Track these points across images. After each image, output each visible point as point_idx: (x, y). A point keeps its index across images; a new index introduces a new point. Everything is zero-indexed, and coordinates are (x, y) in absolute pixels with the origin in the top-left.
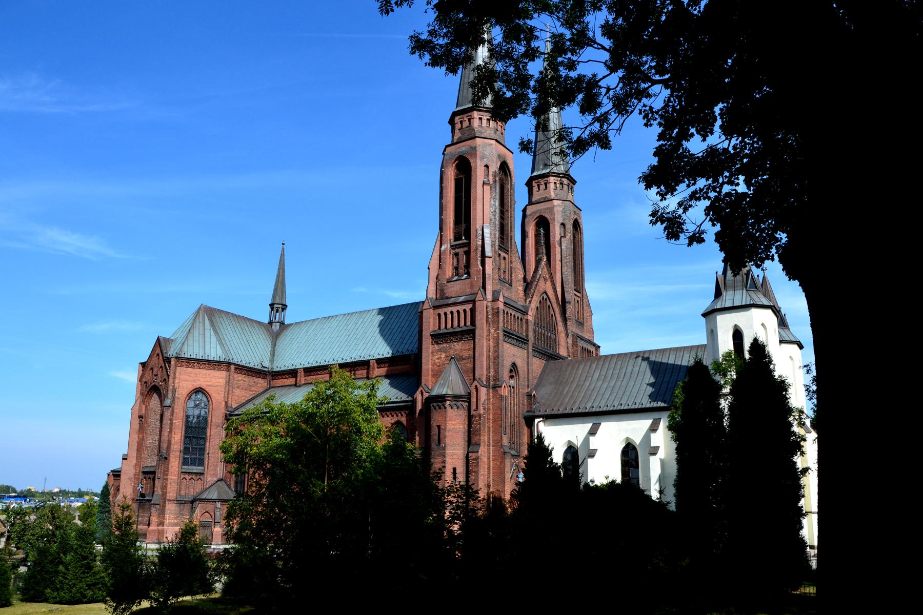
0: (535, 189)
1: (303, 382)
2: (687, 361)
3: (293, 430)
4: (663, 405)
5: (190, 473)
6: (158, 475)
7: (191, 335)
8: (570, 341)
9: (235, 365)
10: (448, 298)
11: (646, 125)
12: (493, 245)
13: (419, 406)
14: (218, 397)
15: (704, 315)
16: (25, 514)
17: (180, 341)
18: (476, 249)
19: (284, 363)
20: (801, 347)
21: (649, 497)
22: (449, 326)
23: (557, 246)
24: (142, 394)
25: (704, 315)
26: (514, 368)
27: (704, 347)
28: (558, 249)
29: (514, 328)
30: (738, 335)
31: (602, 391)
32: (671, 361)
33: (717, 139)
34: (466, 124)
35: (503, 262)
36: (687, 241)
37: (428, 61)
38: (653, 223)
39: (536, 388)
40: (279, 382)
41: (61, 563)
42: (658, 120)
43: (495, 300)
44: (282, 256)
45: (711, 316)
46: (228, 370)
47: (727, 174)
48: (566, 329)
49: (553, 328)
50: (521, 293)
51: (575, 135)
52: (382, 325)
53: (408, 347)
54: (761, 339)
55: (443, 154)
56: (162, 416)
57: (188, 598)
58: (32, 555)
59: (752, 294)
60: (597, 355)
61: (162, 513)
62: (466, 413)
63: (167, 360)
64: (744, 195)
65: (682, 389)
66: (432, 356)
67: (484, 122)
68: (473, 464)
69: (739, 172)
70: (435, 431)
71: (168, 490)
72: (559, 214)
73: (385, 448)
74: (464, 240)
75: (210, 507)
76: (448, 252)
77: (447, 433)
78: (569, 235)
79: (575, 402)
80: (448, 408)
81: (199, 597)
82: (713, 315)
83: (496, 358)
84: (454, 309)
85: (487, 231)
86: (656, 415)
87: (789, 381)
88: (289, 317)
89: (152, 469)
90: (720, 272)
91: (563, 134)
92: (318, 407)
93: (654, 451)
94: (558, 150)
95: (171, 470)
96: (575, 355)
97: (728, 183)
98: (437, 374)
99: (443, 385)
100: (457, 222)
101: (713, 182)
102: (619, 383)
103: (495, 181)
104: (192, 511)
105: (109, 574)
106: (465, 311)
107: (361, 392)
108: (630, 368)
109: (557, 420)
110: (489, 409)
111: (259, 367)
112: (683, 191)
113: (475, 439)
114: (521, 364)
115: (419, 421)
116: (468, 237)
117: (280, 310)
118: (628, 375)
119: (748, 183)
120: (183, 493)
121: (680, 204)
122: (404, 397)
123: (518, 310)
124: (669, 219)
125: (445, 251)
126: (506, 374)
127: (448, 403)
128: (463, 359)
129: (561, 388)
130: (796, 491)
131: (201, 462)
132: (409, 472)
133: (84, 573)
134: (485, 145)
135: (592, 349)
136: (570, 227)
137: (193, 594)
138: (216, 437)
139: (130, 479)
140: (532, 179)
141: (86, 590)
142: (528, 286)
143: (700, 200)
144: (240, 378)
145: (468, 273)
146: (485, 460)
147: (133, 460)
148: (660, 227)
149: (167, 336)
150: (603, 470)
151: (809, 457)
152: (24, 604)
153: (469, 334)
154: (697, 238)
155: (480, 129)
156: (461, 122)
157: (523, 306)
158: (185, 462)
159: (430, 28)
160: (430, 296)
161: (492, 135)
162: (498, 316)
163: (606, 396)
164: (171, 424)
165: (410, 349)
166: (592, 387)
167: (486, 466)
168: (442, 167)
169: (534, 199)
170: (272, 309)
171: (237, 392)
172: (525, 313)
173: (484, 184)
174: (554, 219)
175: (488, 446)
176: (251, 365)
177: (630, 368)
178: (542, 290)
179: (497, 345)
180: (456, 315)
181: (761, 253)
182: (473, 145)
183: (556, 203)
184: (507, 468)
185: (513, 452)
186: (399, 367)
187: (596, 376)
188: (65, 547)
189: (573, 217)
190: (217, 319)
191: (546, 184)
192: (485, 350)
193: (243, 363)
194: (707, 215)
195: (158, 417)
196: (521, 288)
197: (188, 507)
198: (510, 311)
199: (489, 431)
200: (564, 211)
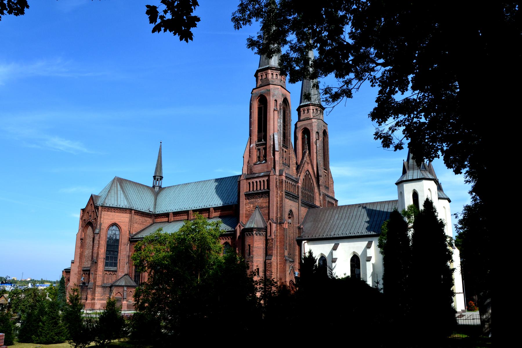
0: (302, 113)
1: (172, 220)
2: (389, 209)
3: (174, 248)
4: (374, 233)
5: (109, 271)
6: (92, 272)
7: (110, 194)
8: (321, 197)
9: (134, 210)
11: (372, 86)
12: (279, 145)
13: (238, 234)
14: (125, 228)
15: (397, 184)
16: (19, 293)
17: (103, 196)
18: (270, 147)
19: (162, 209)
20: (450, 201)
21: (364, 282)
22: (255, 189)
23: (314, 144)
24: (82, 226)
25: (397, 184)
26: (291, 213)
27: (396, 201)
28: (315, 146)
29: (291, 190)
30: (415, 195)
31: (340, 226)
32: (378, 209)
33: (410, 94)
34: (264, 77)
35: (285, 154)
36: (394, 149)
37: (256, 52)
38: (376, 139)
39: (303, 223)
40: (159, 220)
41: (41, 321)
42: (378, 83)
43: (281, 175)
44: (160, 149)
45: (400, 185)
46: (131, 213)
47: (415, 113)
48: (319, 191)
49: (312, 190)
50: (295, 171)
51: (334, 91)
52: (217, 188)
53: (232, 201)
54: (430, 199)
55: (252, 93)
56: (94, 239)
57: (116, 341)
58: (24, 316)
59: (423, 172)
60: (336, 205)
61: (94, 293)
62: (264, 238)
63: (97, 208)
64: (424, 123)
65: (384, 224)
66: (245, 206)
67: (275, 76)
68: (269, 266)
69: (421, 111)
70: (247, 248)
71: (97, 280)
72: (315, 127)
73: (225, 258)
74: (263, 142)
75: (120, 290)
76: (254, 148)
77: (254, 249)
78: (321, 139)
79: (324, 232)
80: (255, 235)
81: (122, 340)
82: (402, 184)
83: (281, 208)
84: (258, 180)
85: (276, 136)
86: (370, 239)
87: (444, 222)
88: (164, 183)
89: (88, 269)
90: (406, 160)
91: (327, 91)
92: (187, 235)
93: (369, 259)
94: (325, 99)
95: (99, 269)
96: (324, 205)
97: (416, 117)
98: (248, 216)
99: (252, 222)
100: (259, 131)
101: (408, 117)
102: (349, 221)
103: (280, 109)
104: (111, 291)
105: (67, 327)
106: (264, 181)
107: (210, 227)
108: (355, 213)
109: (315, 242)
110: (277, 236)
111: (148, 212)
112: (391, 121)
113: (269, 252)
114: (295, 210)
115: (239, 242)
116: (266, 140)
117: (159, 179)
118: (354, 217)
119: (426, 117)
120: (105, 282)
121: (390, 129)
122: (230, 229)
123: (293, 180)
124: (384, 137)
125: (252, 147)
126: (286, 216)
127: (255, 232)
128: (263, 208)
129: (317, 224)
130: (450, 282)
131: (115, 265)
132: (236, 270)
133: (53, 326)
134: (275, 89)
135: (334, 202)
136: (321, 134)
137: (119, 338)
138: (125, 251)
139: (75, 274)
140: (300, 107)
141: (54, 336)
142: (298, 167)
143: (401, 126)
144: (137, 218)
145: (266, 160)
146: (275, 264)
147: (77, 264)
148: (380, 141)
149: (97, 194)
150: (341, 270)
151: (456, 262)
152: (20, 344)
153: (266, 194)
154: (399, 147)
156: (262, 76)
157: (296, 178)
158: (106, 265)
159: (259, 34)
160: (244, 173)
161: (279, 83)
162: (282, 184)
163: (342, 228)
164: (99, 243)
165: (232, 202)
166: (334, 224)
167: (275, 267)
168: (251, 100)
169: (302, 118)
170: (155, 179)
171: (136, 225)
172: (297, 182)
173: (274, 110)
174: (312, 130)
175: (277, 256)
176: (143, 211)
177: (355, 213)
178: (306, 169)
179: (282, 200)
180: (259, 183)
181: (432, 154)
182: (268, 89)
183: (313, 120)
184: (287, 269)
185: (291, 260)
186: (226, 212)
187: (336, 217)
188: (42, 312)
189: (323, 128)
190: (124, 184)
191: (308, 110)
192: (275, 203)
193: (139, 209)
194: (404, 134)
195: (92, 239)
196: (295, 168)
197: (108, 290)
198: (289, 181)
199: (277, 248)
200: (318, 125)
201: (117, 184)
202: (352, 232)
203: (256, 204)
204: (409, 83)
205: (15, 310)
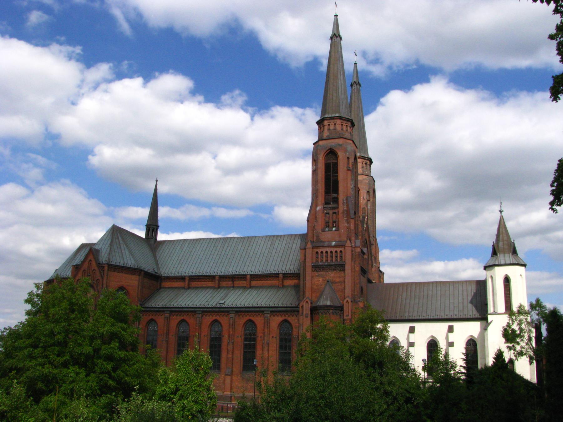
10: (322, 242)
34: (332, 127)
67: (344, 127)
84: (329, 250)
128: (336, 283)
155: (342, 132)
201: (117, 236)
203: (327, 278)
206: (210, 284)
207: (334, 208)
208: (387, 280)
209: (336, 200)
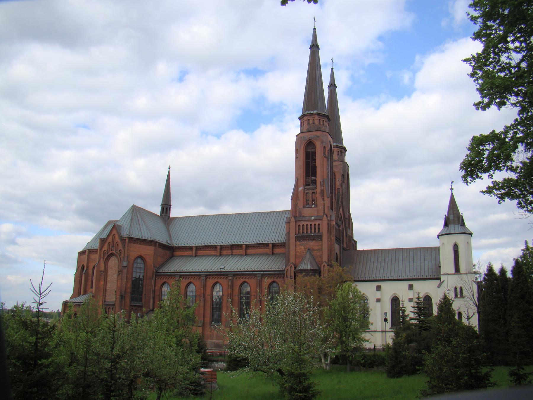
8: (347, 239)
46: (155, 246)
84: (309, 223)
144: (160, 250)
158: (132, 299)
176: (146, 238)
177: (277, 236)
202: (392, 275)
204: (487, 158)
205: (124, 372)
206: (213, 252)
207: (313, 189)
208: (359, 247)
209: (314, 182)
